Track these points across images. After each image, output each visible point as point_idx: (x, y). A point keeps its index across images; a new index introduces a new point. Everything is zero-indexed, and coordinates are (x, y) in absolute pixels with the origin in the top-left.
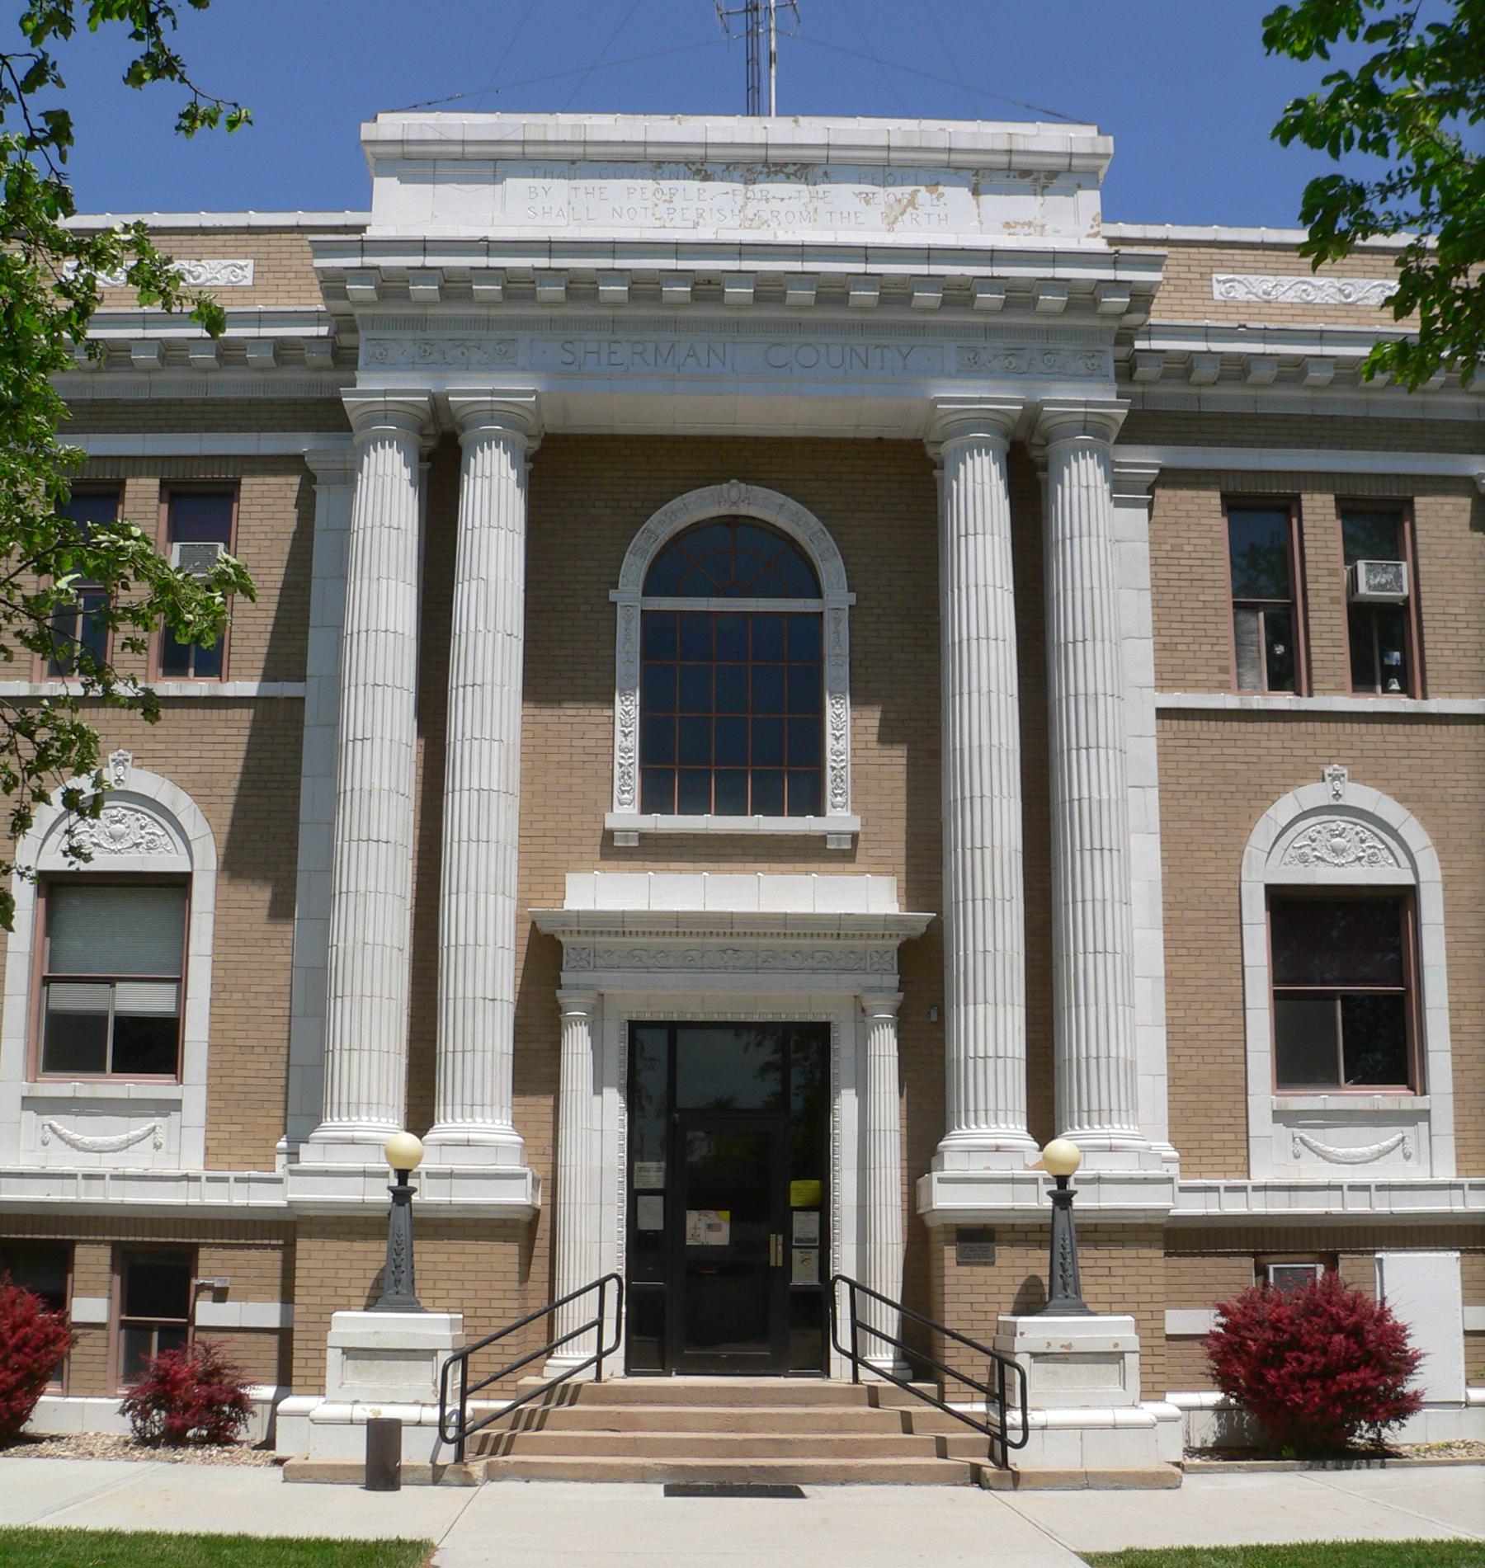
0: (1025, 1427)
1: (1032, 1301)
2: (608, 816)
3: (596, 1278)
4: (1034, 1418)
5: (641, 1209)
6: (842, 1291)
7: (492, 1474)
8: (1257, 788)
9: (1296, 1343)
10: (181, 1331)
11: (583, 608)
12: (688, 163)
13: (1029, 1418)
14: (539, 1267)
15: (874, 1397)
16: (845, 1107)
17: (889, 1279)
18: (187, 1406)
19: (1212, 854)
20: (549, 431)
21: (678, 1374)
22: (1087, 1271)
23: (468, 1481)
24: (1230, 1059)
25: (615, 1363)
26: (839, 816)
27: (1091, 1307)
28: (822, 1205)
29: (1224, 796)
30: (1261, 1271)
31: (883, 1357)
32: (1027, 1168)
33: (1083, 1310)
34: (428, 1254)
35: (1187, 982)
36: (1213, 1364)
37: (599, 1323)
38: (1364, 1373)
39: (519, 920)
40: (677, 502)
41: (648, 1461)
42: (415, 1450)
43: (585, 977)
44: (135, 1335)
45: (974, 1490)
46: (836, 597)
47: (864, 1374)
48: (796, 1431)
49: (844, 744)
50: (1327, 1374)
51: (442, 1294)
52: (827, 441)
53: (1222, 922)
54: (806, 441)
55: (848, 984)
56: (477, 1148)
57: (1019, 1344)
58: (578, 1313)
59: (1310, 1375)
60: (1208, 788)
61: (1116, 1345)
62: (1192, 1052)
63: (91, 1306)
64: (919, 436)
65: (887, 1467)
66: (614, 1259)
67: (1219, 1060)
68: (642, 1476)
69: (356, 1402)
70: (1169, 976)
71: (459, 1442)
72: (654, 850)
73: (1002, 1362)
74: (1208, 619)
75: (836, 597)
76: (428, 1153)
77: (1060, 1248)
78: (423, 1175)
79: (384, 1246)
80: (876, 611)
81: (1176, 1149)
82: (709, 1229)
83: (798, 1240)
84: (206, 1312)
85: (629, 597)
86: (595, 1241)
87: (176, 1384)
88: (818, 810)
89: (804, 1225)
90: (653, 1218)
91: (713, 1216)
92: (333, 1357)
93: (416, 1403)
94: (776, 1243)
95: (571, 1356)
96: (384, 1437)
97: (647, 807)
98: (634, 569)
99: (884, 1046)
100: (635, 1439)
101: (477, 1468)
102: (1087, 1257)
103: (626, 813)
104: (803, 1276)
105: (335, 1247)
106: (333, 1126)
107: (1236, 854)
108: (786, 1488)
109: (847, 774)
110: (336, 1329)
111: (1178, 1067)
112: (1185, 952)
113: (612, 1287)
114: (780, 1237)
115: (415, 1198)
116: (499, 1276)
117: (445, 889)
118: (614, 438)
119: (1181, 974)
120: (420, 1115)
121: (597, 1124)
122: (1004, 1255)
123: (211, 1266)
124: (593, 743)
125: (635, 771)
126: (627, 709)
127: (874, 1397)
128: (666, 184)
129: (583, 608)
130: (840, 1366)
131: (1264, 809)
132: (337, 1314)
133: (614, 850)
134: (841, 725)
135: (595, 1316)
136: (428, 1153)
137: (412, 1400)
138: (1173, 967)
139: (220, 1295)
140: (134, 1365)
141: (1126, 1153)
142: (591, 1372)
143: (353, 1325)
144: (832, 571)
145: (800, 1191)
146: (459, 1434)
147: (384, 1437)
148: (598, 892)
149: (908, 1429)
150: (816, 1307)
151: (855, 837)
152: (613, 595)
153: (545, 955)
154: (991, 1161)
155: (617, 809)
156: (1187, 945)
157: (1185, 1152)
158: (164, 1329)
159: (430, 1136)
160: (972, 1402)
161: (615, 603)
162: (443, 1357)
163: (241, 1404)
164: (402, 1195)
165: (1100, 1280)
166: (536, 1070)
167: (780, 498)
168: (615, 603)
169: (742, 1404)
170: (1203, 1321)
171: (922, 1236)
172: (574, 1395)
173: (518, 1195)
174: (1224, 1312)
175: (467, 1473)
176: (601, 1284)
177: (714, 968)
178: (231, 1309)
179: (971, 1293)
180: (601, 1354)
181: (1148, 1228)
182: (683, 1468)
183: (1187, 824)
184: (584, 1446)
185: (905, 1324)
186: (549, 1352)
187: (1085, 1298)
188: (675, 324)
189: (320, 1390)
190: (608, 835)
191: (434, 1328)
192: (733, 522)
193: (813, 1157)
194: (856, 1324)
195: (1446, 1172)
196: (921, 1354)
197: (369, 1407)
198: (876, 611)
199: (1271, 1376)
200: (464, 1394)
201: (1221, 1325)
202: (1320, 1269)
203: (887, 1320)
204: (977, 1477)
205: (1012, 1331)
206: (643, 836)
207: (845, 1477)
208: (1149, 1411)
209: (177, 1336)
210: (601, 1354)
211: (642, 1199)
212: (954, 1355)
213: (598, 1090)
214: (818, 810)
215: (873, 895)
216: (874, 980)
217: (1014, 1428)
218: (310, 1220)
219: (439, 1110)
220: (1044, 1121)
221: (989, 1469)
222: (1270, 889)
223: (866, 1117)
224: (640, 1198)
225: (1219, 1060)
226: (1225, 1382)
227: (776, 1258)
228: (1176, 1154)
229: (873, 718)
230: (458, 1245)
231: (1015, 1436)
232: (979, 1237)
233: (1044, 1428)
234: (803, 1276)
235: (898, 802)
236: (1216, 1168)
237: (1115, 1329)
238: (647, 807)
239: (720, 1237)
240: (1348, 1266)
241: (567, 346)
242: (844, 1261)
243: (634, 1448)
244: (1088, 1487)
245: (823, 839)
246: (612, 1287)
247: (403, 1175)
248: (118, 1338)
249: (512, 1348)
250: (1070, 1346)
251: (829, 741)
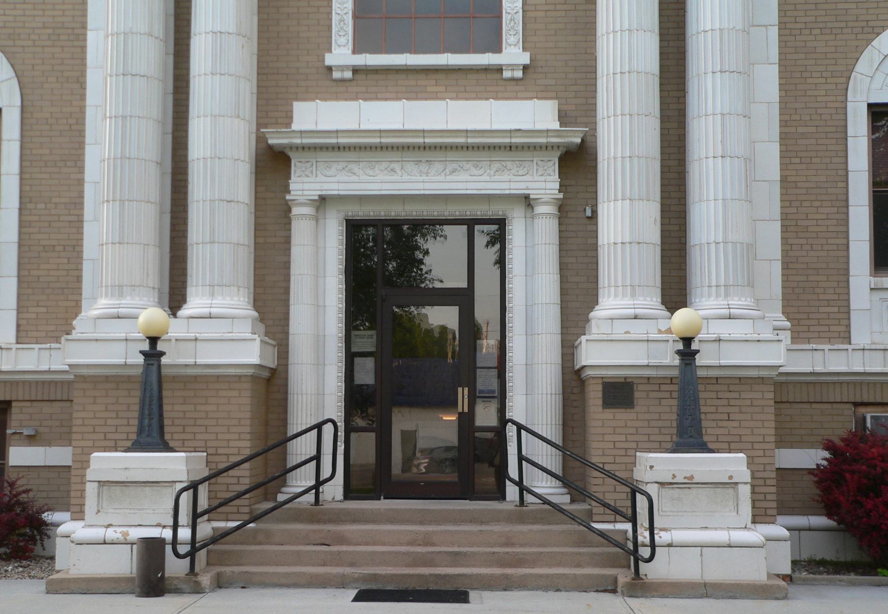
0: (653, 545)
3: (314, 422)
4: (662, 537)
5: (357, 368)
6: (511, 431)
7: (220, 584)
8: (864, 24)
10: (691, 364)
13: (656, 537)
19: (823, 80)
21: (385, 498)
22: (709, 416)
23: (198, 590)
24: (835, 247)
25: (334, 490)
26: (513, 54)
27: (710, 446)
29: (834, 31)
32: (660, 332)
33: (703, 448)
35: (799, 185)
36: (818, 492)
37: (317, 458)
41: (348, 570)
47: (529, 498)
48: (472, 545)
51: (191, 436)
53: (830, 135)
58: (303, 448)
60: (821, 25)
61: (731, 477)
62: (804, 241)
65: (541, 576)
67: (826, 247)
68: (341, 583)
69: (109, 526)
70: (784, 180)
74: (27, 13)
76: (176, 329)
77: (689, 401)
78: (173, 340)
81: (788, 320)
83: (480, 392)
88: (497, 48)
92: (91, 490)
93: (158, 525)
97: (357, 49)
100: (339, 552)
103: (342, 54)
107: (843, 80)
110: (93, 465)
111: (790, 253)
112: (798, 160)
113: (328, 429)
114: (466, 390)
115: (164, 360)
116: (235, 422)
119: (793, 179)
130: (512, 491)
131: (869, 42)
132: (95, 454)
135: (314, 452)
136: (176, 329)
138: (787, 173)
139: (32, 440)
141: (740, 325)
142: (310, 497)
154: (627, 331)
156: (800, 154)
157: (796, 322)
160: (615, 522)
162: (179, 486)
165: (720, 424)
169: (430, 523)
170: (813, 457)
171: (573, 380)
175: (196, 582)
176: (319, 427)
182: (375, 577)
183: (802, 56)
187: (705, 438)
194: (521, 458)
196: (574, 472)
197: (119, 530)
200: (196, 516)
201: (826, 459)
206: (356, 70)
207: (506, 585)
208: (756, 535)
211: (357, 360)
212: (598, 485)
217: (644, 545)
224: (357, 360)
225: (826, 247)
228: (788, 324)
231: (645, 552)
232: (620, 392)
233: (670, 545)
236: (822, 335)
237: (733, 464)
238: (357, 49)
242: (516, 409)
243: (338, 560)
244: (707, 596)
250: (692, 477)
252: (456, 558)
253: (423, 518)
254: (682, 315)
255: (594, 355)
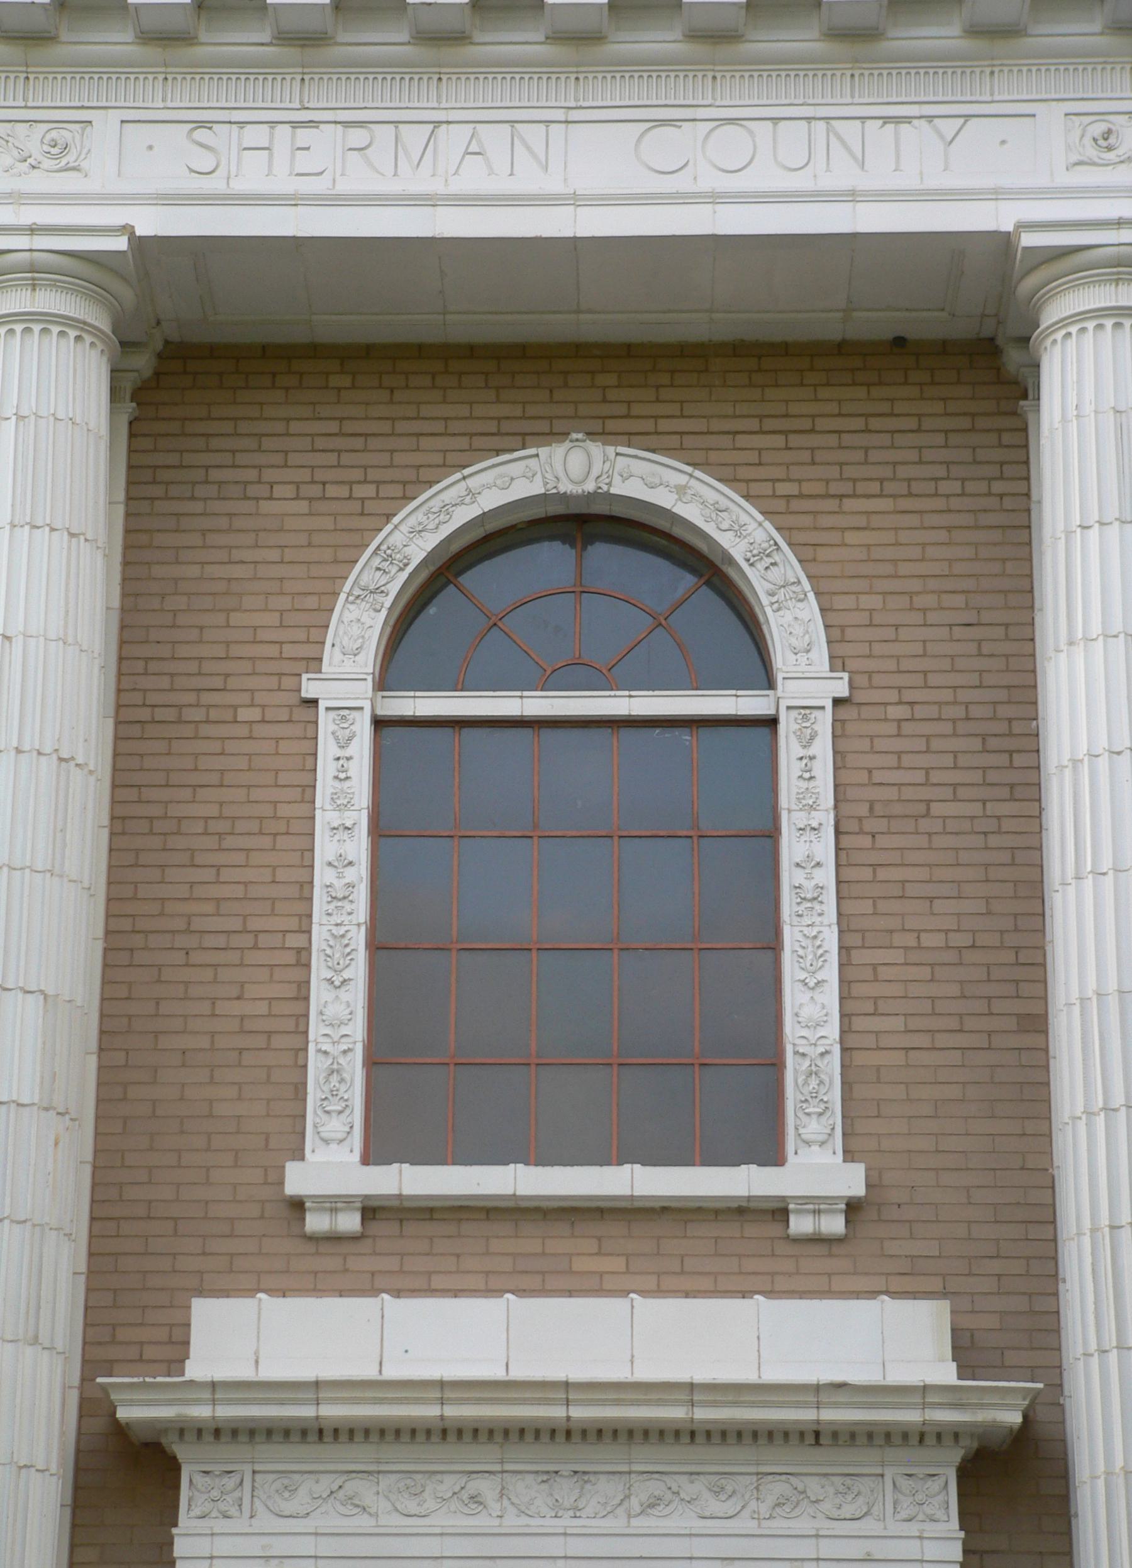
2: (292, 1169)
11: (244, 714)
20: (175, 337)
26: (816, 1169)
46: (805, 671)
64: (987, 333)
75: (805, 671)
80: (895, 712)
88: (774, 1156)
97: (373, 1154)
98: (356, 630)
103: (331, 1165)
124: (262, 1008)
129: (244, 714)
144: (795, 626)
155: (316, 1153)
161: (314, 702)
168: (314, 702)
198: (895, 712)
206: (372, 1210)
214: (774, 1156)
222: (366, 1160)
238: (373, 1154)
241: (201, 135)
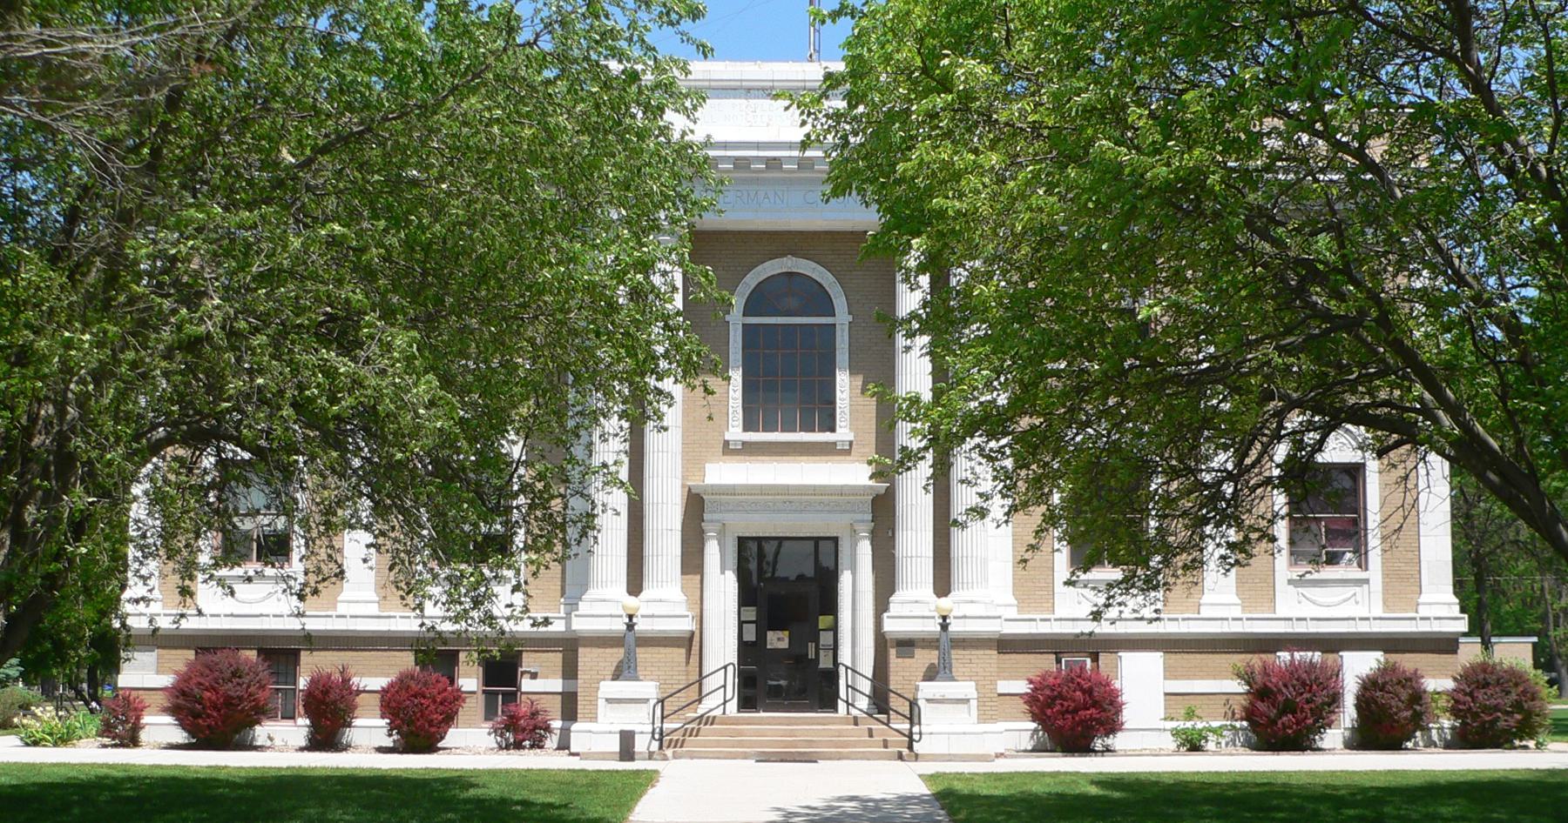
1: (931, 675)
6: (842, 670)
9: (1061, 696)
10: (514, 694)
12: (763, 89)
14: (694, 659)
15: (856, 721)
16: (845, 579)
17: (867, 666)
18: (524, 730)
23: (665, 758)
25: (732, 706)
28: (835, 629)
30: (1059, 661)
31: (863, 703)
33: (953, 679)
34: (643, 654)
38: (1093, 711)
39: (683, 486)
40: (760, 268)
42: (641, 744)
43: (716, 516)
44: (490, 697)
45: (899, 762)
49: (846, 395)
50: (1076, 711)
52: (838, 232)
54: (826, 233)
55: (846, 519)
56: (664, 603)
57: (920, 695)
58: (711, 683)
59: (1067, 711)
63: (469, 681)
66: (732, 656)
68: (745, 756)
71: (661, 740)
72: (749, 449)
73: (913, 704)
77: (944, 649)
79: (622, 651)
82: (778, 640)
84: (527, 685)
85: (736, 319)
86: (722, 647)
87: (519, 719)
88: (832, 429)
89: (826, 638)
90: (751, 635)
91: (780, 634)
92: (601, 703)
94: (811, 647)
95: (710, 704)
96: (627, 738)
97: (746, 428)
98: (738, 302)
99: (865, 550)
101: (669, 752)
102: (956, 654)
103: (735, 432)
104: (825, 663)
105: (597, 651)
106: (591, 594)
108: (810, 759)
109: (847, 411)
113: (730, 669)
117: (646, 475)
118: (727, 232)
120: (635, 584)
121: (723, 587)
122: (918, 652)
123: (529, 662)
125: (740, 410)
126: (737, 376)
127: (856, 721)
128: (752, 101)
130: (841, 706)
133: (728, 449)
134: (844, 384)
137: (640, 721)
139: (534, 676)
140: (490, 713)
143: (609, 688)
144: (840, 303)
145: (824, 621)
146: (661, 737)
147: (627, 738)
148: (723, 473)
149: (871, 736)
150: (832, 676)
151: (851, 443)
152: (727, 318)
153: (695, 505)
154: (914, 610)
158: (504, 694)
159: (643, 595)
162: (653, 702)
163: (548, 729)
164: (630, 627)
166: (692, 562)
167: (814, 265)
170: (1023, 687)
171: (882, 642)
172: (713, 721)
173: (686, 625)
174: (1031, 682)
176: (725, 667)
177: (779, 511)
178: (540, 682)
179: (902, 670)
180: (725, 702)
181: (990, 640)
184: (718, 744)
185: (874, 689)
186: (700, 701)
188: (758, 181)
189: (594, 719)
190: (727, 443)
191: (647, 689)
192: (790, 275)
193: (829, 605)
195: (1378, 611)
196: (880, 701)
199: (1049, 712)
202: (1089, 661)
203: (865, 686)
204: (900, 757)
205: (917, 689)
206: (744, 443)
207: (840, 757)
209: (511, 697)
210: (725, 702)
212: (895, 702)
213: (723, 572)
215: (856, 474)
216: (859, 516)
218: (584, 638)
219: (645, 584)
220: (943, 585)
221: (905, 751)
223: (855, 584)
226: (1035, 718)
227: (811, 655)
229: (859, 381)
230: (656, 649)
231: (916, 737)
232: (907, 645)
234: (825, 663)
235: (872, 425)
237: (966, 688)
238: (746, 428)
239: (784, 645)
240: (1103, 658)
242: (845, 656)
243: (741, 744)
245: (835, 444)
246: (730, 669)
247: (631, 617)
248: (481, 698)
249: (683, 699)
251: (838, 394)
252: (810, 743)
253: (790, 722)
254: (945, 603)
255: (889, 626)
